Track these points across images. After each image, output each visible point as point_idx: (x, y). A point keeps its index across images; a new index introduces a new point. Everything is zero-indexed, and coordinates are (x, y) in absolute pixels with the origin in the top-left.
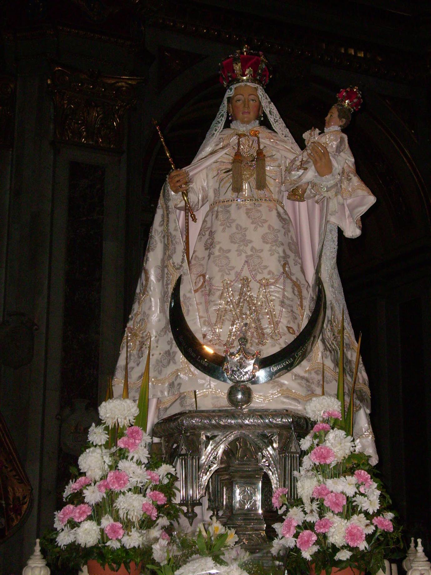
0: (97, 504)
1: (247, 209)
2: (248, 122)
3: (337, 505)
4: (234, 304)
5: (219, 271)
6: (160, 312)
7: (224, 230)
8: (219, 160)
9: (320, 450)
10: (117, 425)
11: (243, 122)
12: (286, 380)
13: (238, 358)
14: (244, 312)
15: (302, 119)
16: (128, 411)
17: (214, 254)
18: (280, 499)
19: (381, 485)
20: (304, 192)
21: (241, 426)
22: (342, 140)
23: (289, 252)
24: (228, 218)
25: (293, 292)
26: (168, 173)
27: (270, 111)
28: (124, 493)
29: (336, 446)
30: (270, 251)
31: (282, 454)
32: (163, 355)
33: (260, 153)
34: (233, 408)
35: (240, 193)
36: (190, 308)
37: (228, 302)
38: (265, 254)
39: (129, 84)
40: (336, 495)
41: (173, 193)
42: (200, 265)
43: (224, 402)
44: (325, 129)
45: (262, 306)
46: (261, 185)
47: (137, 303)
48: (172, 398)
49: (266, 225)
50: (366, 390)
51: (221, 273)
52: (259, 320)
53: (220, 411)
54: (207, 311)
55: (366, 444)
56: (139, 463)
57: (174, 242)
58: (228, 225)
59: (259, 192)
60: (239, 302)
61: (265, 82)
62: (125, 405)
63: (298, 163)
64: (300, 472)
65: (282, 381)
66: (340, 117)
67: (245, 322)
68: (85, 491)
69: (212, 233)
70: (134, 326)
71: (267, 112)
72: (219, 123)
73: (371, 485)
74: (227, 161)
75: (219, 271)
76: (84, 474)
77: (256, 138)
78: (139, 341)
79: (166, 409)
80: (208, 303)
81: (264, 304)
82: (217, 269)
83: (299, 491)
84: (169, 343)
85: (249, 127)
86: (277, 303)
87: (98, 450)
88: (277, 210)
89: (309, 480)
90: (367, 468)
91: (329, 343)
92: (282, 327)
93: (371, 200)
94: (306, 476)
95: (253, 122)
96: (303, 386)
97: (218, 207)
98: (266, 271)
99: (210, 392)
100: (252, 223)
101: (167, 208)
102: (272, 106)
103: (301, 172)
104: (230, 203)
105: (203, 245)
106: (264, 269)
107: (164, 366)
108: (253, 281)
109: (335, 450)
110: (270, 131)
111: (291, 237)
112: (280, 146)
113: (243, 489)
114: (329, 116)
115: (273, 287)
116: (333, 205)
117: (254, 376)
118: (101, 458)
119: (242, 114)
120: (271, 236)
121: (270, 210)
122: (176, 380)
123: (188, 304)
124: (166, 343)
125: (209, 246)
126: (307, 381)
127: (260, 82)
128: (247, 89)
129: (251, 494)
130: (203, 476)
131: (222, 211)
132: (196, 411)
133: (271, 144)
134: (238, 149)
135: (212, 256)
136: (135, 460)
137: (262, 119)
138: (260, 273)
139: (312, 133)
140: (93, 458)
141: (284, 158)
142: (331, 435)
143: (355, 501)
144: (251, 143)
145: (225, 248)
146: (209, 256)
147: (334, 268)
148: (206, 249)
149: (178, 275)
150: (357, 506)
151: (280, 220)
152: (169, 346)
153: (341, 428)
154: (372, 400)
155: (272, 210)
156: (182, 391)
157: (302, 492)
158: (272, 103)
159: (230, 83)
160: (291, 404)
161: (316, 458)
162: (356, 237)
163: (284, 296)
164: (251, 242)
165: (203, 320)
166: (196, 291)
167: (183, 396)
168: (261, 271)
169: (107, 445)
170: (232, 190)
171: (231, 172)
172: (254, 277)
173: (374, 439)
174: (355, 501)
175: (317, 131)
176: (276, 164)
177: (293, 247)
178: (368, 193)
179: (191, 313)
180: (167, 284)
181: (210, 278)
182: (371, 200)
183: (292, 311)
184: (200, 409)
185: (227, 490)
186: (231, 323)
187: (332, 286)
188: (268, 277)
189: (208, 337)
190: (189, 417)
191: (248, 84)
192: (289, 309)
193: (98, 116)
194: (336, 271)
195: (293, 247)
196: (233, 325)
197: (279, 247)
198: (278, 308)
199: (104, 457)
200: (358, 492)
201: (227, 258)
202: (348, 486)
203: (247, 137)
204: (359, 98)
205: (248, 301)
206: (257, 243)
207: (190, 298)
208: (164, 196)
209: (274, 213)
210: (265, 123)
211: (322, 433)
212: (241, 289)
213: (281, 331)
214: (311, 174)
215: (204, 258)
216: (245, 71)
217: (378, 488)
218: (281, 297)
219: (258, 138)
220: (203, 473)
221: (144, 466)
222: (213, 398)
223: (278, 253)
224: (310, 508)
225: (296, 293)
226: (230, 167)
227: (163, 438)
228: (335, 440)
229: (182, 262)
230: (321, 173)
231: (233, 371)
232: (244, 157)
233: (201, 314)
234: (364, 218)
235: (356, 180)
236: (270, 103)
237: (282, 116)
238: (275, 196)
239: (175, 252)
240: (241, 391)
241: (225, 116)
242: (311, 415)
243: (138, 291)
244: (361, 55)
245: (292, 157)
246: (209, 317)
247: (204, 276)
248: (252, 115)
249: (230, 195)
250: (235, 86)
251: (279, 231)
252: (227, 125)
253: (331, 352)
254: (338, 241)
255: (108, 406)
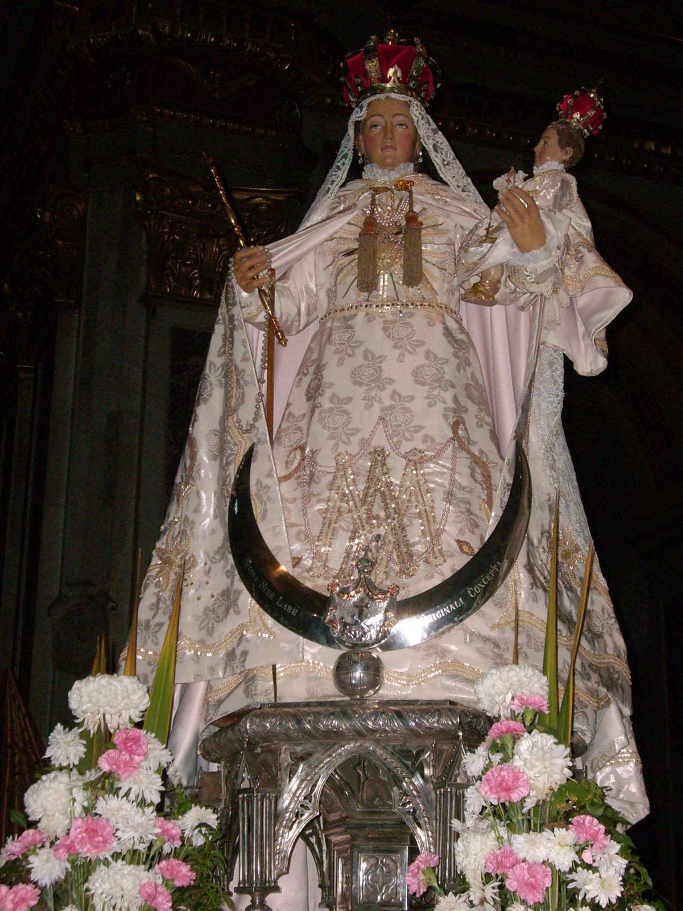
0: (57, 885)
1: (385, 322)
2: (392, 167)
3: (533, 887)
4: (357, 499)
5: (330, 438)
6: (216, 517)
7: (341, 362)
8: (337, 235)
9: (499, 774)
10: (102, 726)
11: (383, 165)
12: (455, 643)
13: (355, 599)
14: (374, 513)
15: (491, 151)
16: (124, 698)
17: (321, 406)
18: (422, 877)
19: (630, 847)
20: (495, 289)
21: (359, 734)
22: (565, 184)
23: (465, 402)
24: (349, 340)
25: (473, 476)
26: (232, 253)
27: (434, 146)
28: (106, 863)
29: (533, 767)
30: (427, 398)
31: (439, 788)
32: (217, 599)
33: (412, 218)
34: (347, 698)
35: (374, 293)
36: (269, 506)
37: (344, 495)
38: (418, 405)
39: (271, 200)
40: (530, 867)
41: (245, 294)
42: (295, 429)
43: (328, 689)
44: (535, 168)
45: (409, 501)
46: (413, 275)
47: (175, 501)
48: (232, 680)
49: (421, 351)
50: (622, 669)
51: (332, 442)
52: (403, 529)
53: (320, 704)
54: (304, 511)
55: (625, 776)
56: (142, 803)
57: (242, 382)
58: (350, 352)
59: (411, 289)
60: (366, 495)
61: (426, 95)
62: (119, 687)
63: (482, 232)
64: (464, 821)
65: (445, 645)
66: (562, 145)
67: (375, 532)
68: (31, 858)
69: (319, 369)
70: (167, 545)
71: (430, 148)
72: (340, 169)
73: (605, 846)
74: (351, 237)
75: (330, 438)
76: (33, 825)
77: (408, 194)
78: (175, 574)
79: (220, 702)
80: (307, 498)
81: (413, 499)
82: (326, 433)
83: (459, 859)
84: (229, 574)
85: (395, 175)
86: (439, 496)
87: (63, 777)
88: (444, 323)
89: (479, 837)
90: (600, 812)
91: (542, 574)
92: (448, 541)
93: (624, 297)
94: (476, 831)
95: (402, 165)
96: (486, 656)
97: (333, 323)
98: (418, 437)
99: (302, 668)
100: (395, 347)
101: (232, 318)
102: (440, 137)
103: (486, 246)
104: (353, 311)
105: (305, 391)
106: (416, 432)
107: (219, 620)
108: (393, 454)
109: (531, 774)
110: (437, 182)
111: (473, 375)
112: (451, 208)
113: (373, 861)
114: (542, 143)
115: (432, 465)
116: (554, 308)
117: (385, 634)
118: (67, 793)
119: (382, 150)
120: (431, 372)
121: (430, 324)
122: (238, 645)
123: (265, 498)
124: (224, 576)
125: (313, 394)
126: (496, 645)
127: (416, 92)
128: (394, 107)
129: (389, 872)
130: (283, 833)
131: (339, 328)
132: (275, 705)
133: (434, 203)
134: (372, 212)
135: (317, 411)
136: (132, 796)
137: (421, 160)
138: (407, 439)
139: (512, 179)
140: (51, 791)
141: (460, 230)
142: (525, 744)
143: (573, 881)
144: (397, 202)
145: (342, 395)
146: (312, 412)
147: (557, 434)
148: (308, 399)
149: (249, 445)
150: (576, 891)
151: (449, 342)
152: (229, 580)
153: (549, 731)
154: (634, 688)
155: (434, 324)
156: (248, 667)
157: (466, 862)
158: (440, 132)
159: (361, 96)
160: (461, 691)
161: (491, 789)
162: (598, 374)
163: (453, 482)
164: (391, 381)
165: (294, 530)
166: (286, 478)
167: (251, 675)
168: (409, 437)
169: (85, 765)
170: (358, 286)
171: (356, 256)
172: (396, 447)
173: (640, 766)
174: (573, 881)
175: (521, 174)
176: (444, 239)
177: (476, 393)
178: (616, 282)
179: (269, 516)
180: (228, 464)
181: (313, 452)
182: (624, 297)
183: (469, 511)
184: (282, 701)
185: (344, 865)
186: (349, 534)
187: (553, 467)
188: (422, 447)
189: (305, 562)
190: (257, 716)
191: (393, 95)
192: (463, 507)
193: (220, 253)
194: (562, 439)
195: (476, 393)
196: (352, 539)
197: (445, 391)
198: (440, 505)
199: (75, 791)
200: (579, 862)
201: (346, 413)
202: (558, 847)
203: (389, 193)
204: (597, 109)
205: (383, 493)
206: (405, 384)
207: (269, 488)
208: (227, 299)
209: (439, 329)
210: (427, 168)
211: (508, 738)
212: (371, 470)
213: (445, 548)
214: (503, 250)
215: (304, 415)
216: (387, 70)
217: (621, 853)
218: (447, 484)
219: (411, 193)
220: (285, 827)
221: (152, 808)
222: (309, 680)
223: (444, 402)
224: (479, 894)
225: (479, 477)
226: (355, 246)
227: (223, 763)
228: (531, 753)
229: (255, 419)
230: (523, 248)
231: (345, 625)
232: (384, 228)
233: (294, 519)
234: (613, 330)
235: (592, 259)
236: (435, 132)
237: (458, 156)
238: (442, 299)
239: (243, 402)
240: (360, 661)
241: (350, 156)
242: (487, 706)
243: (178, 479)
244: (668, 151)
245: (470, 223)
246: (307, 525)
247: (302, 448)
248: (400, 152)
249: (354, 296)
250: (368, 100)
251: (447, 361)
252: (356, 172)
253: (545, 590)
254: (565, 382)
255: (84, 689)
